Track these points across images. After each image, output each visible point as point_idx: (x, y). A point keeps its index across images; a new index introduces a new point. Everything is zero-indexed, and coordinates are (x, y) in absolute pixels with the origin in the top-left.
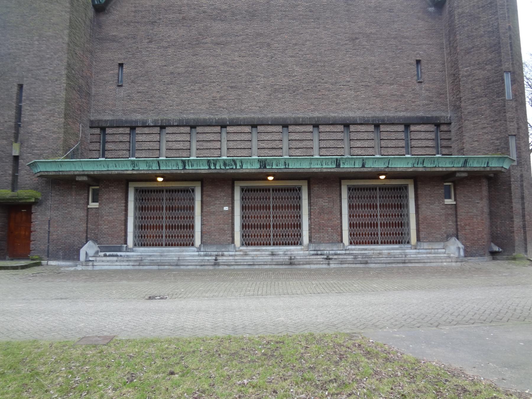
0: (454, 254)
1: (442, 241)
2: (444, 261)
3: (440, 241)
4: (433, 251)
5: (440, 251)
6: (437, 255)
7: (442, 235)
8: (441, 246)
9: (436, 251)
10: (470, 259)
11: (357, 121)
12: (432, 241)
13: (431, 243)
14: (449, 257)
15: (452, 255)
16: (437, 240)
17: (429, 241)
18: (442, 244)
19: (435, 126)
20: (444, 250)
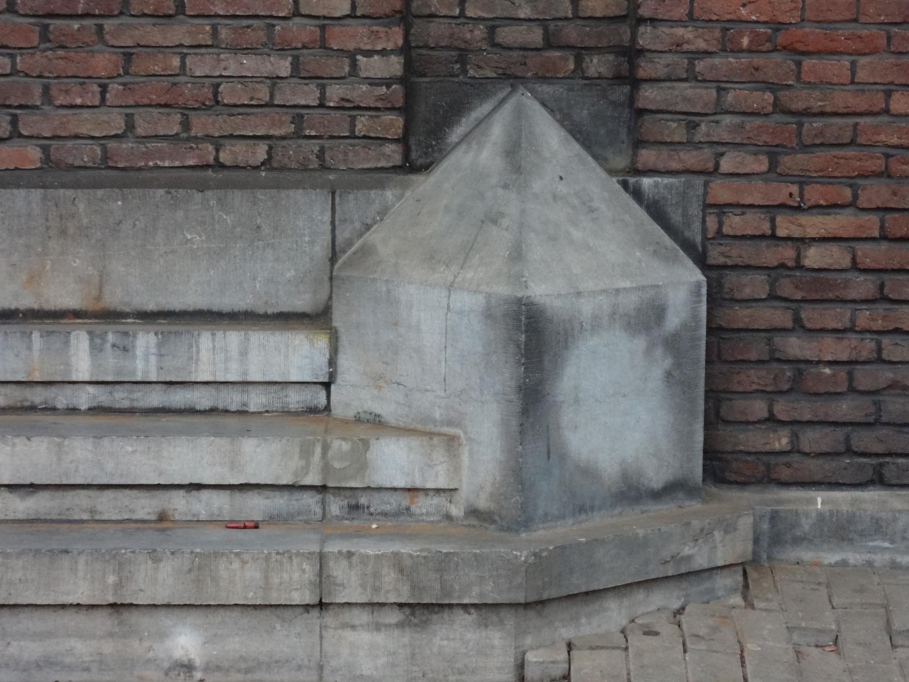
0: (443, 437)
1: (319, 173)
2: (159, 580)
3: (274, 173)
4: (81, 357)
5: (216, 356)
6: (83, 456)
7: (316, 49)
8: (279, 272)
9: (146, 354)
10: (840, 530)
11: (768, 247)
12: (111, 172)
13: (82, 203)
14: (347, 500)
15: (394, 462)
16: (206, 158)
17: (53, 172)
18: (306, 217)
19: (803, 266)
20: (296, 356)
